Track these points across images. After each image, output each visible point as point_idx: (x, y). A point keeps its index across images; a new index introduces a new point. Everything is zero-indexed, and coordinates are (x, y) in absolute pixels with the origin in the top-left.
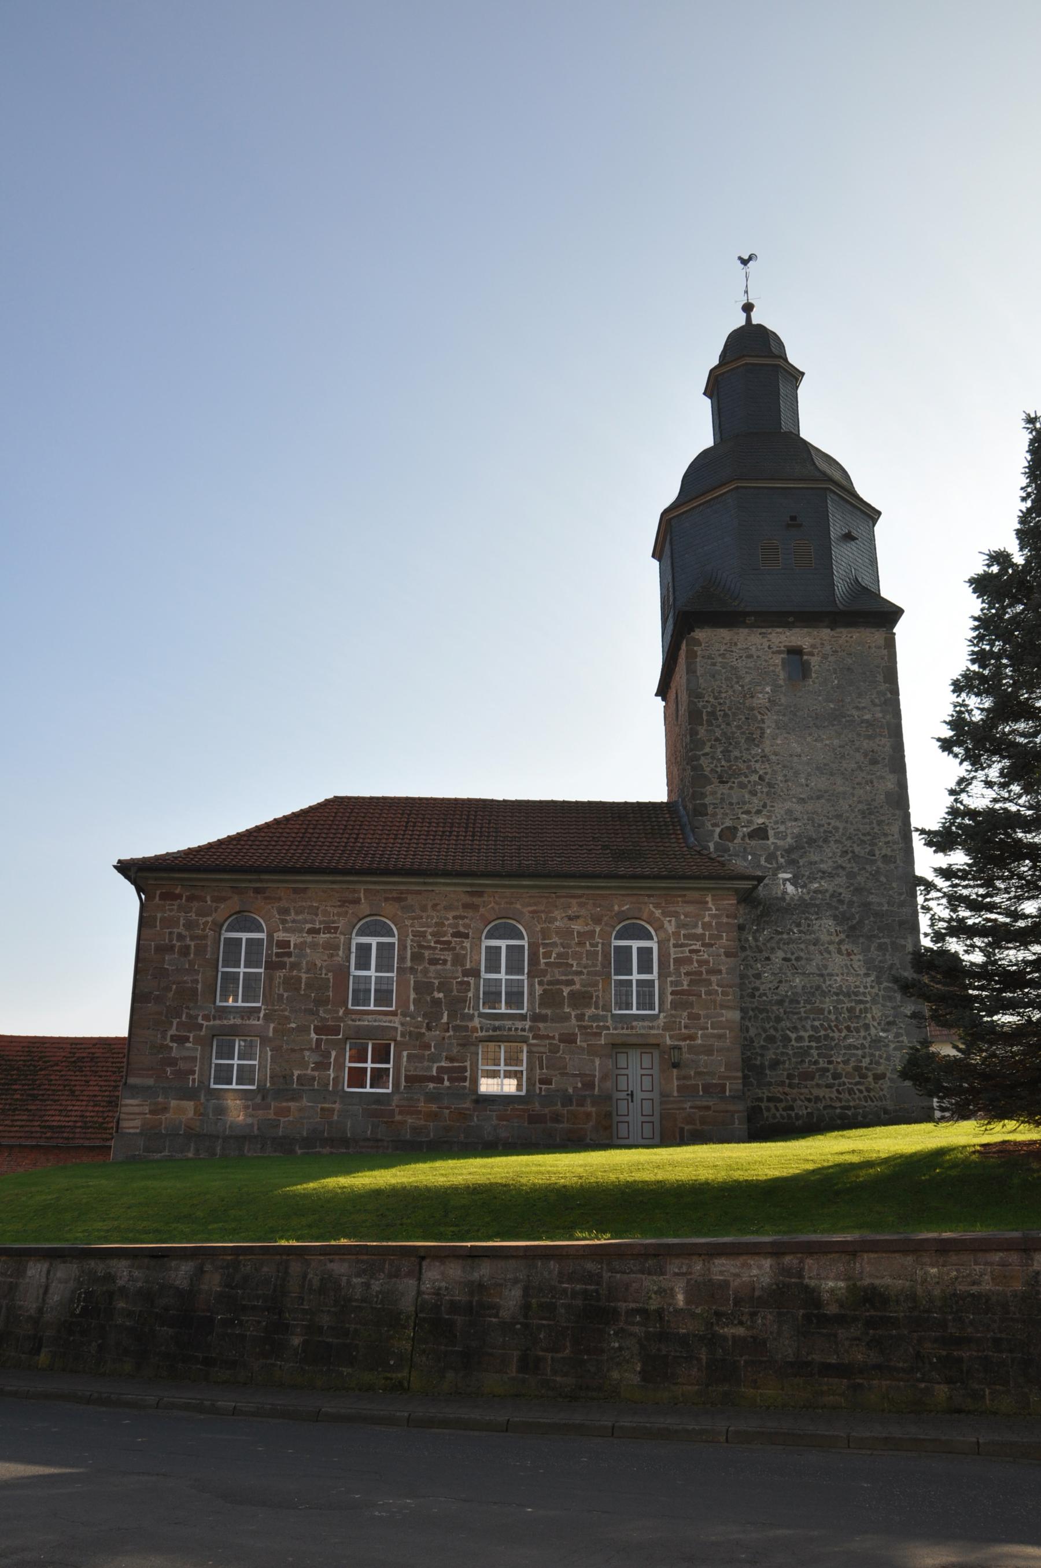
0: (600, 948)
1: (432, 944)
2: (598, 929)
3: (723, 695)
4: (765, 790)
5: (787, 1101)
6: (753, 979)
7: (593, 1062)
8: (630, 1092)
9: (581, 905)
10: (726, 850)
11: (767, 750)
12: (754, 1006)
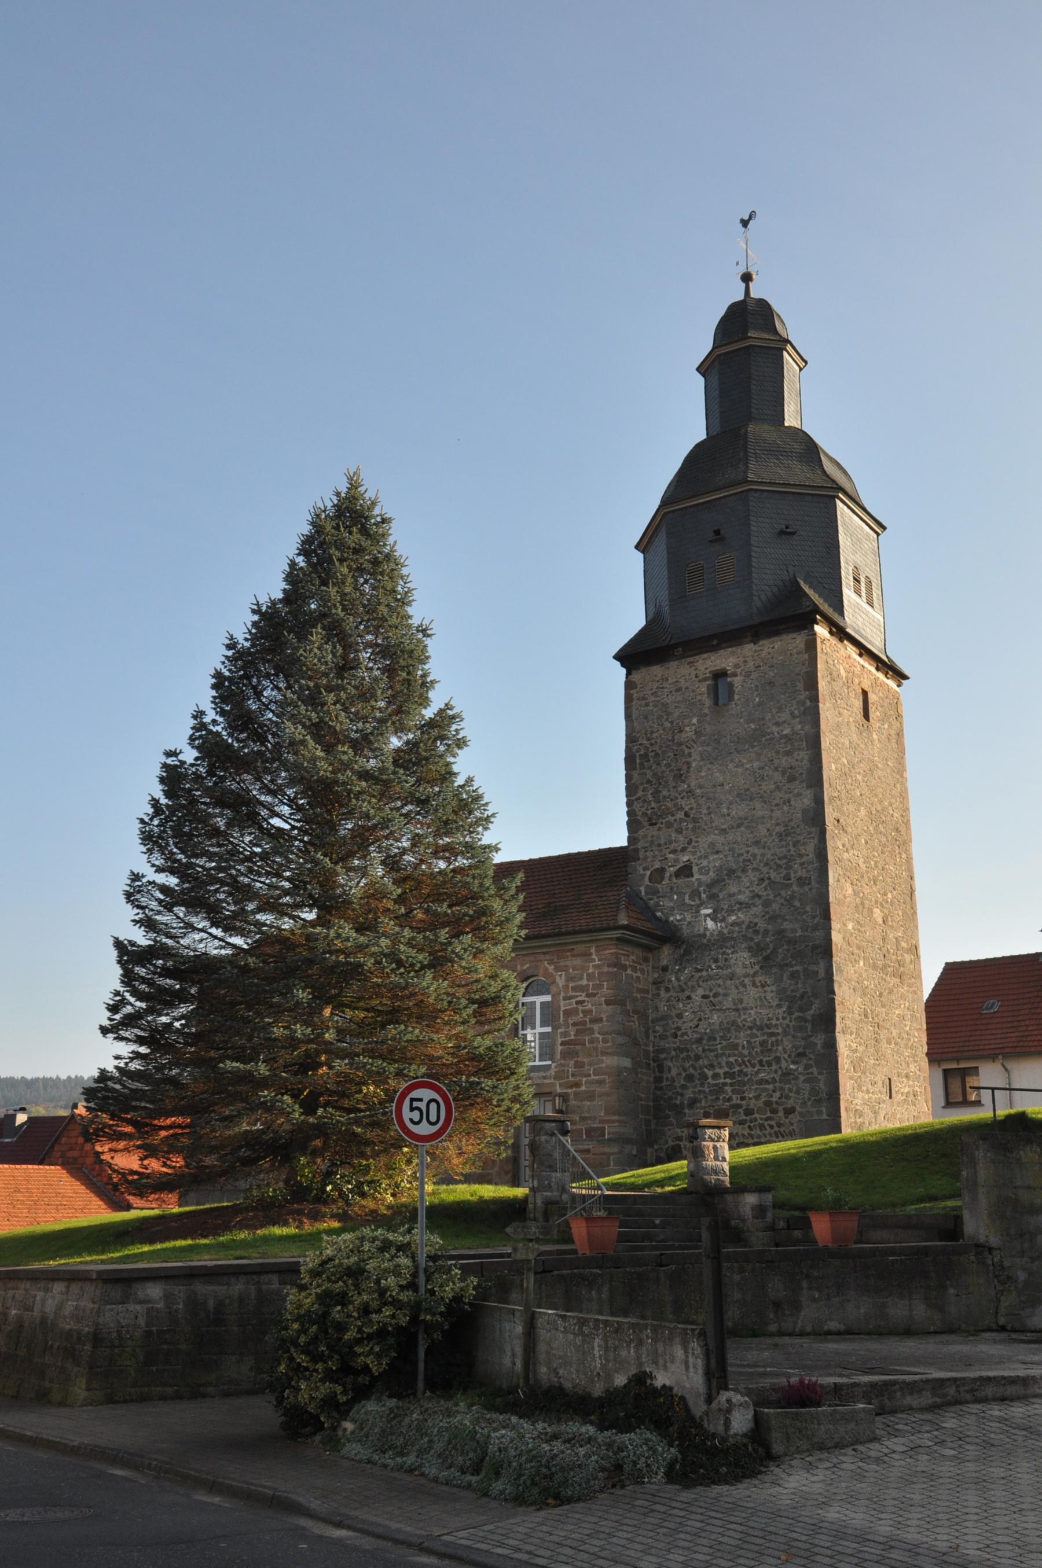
3: (655, 735)
4: (690, 826)
6: (676, 1019)
10: (656, 892)
11: (693, 784)
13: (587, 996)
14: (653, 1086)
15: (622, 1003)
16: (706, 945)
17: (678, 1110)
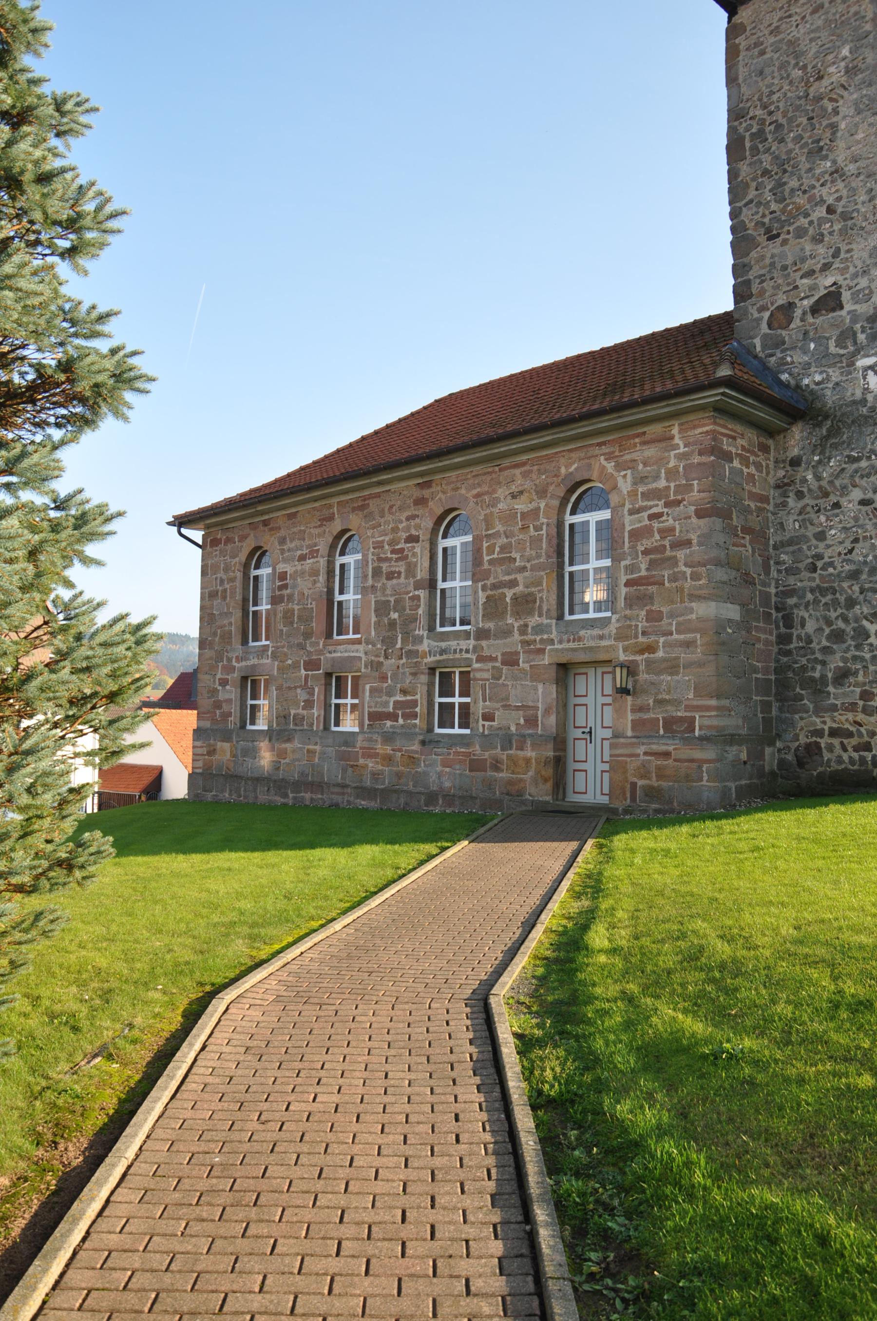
0: (544, 532)
1: (389, 555)
2: (542, 505)
3: (775, 97)
4: (837, 227)
5: (860, 735)
6: (814, 542)
7: (536, 689)
8: (588, 730)
9: (525, 475)
10: (779, 343)
11: (840, 160)
12: (814, 584)
13: (667, 505)
14: (775, 649)
15: (725, 515)
16: (866, 417)
17: (818, 688)
